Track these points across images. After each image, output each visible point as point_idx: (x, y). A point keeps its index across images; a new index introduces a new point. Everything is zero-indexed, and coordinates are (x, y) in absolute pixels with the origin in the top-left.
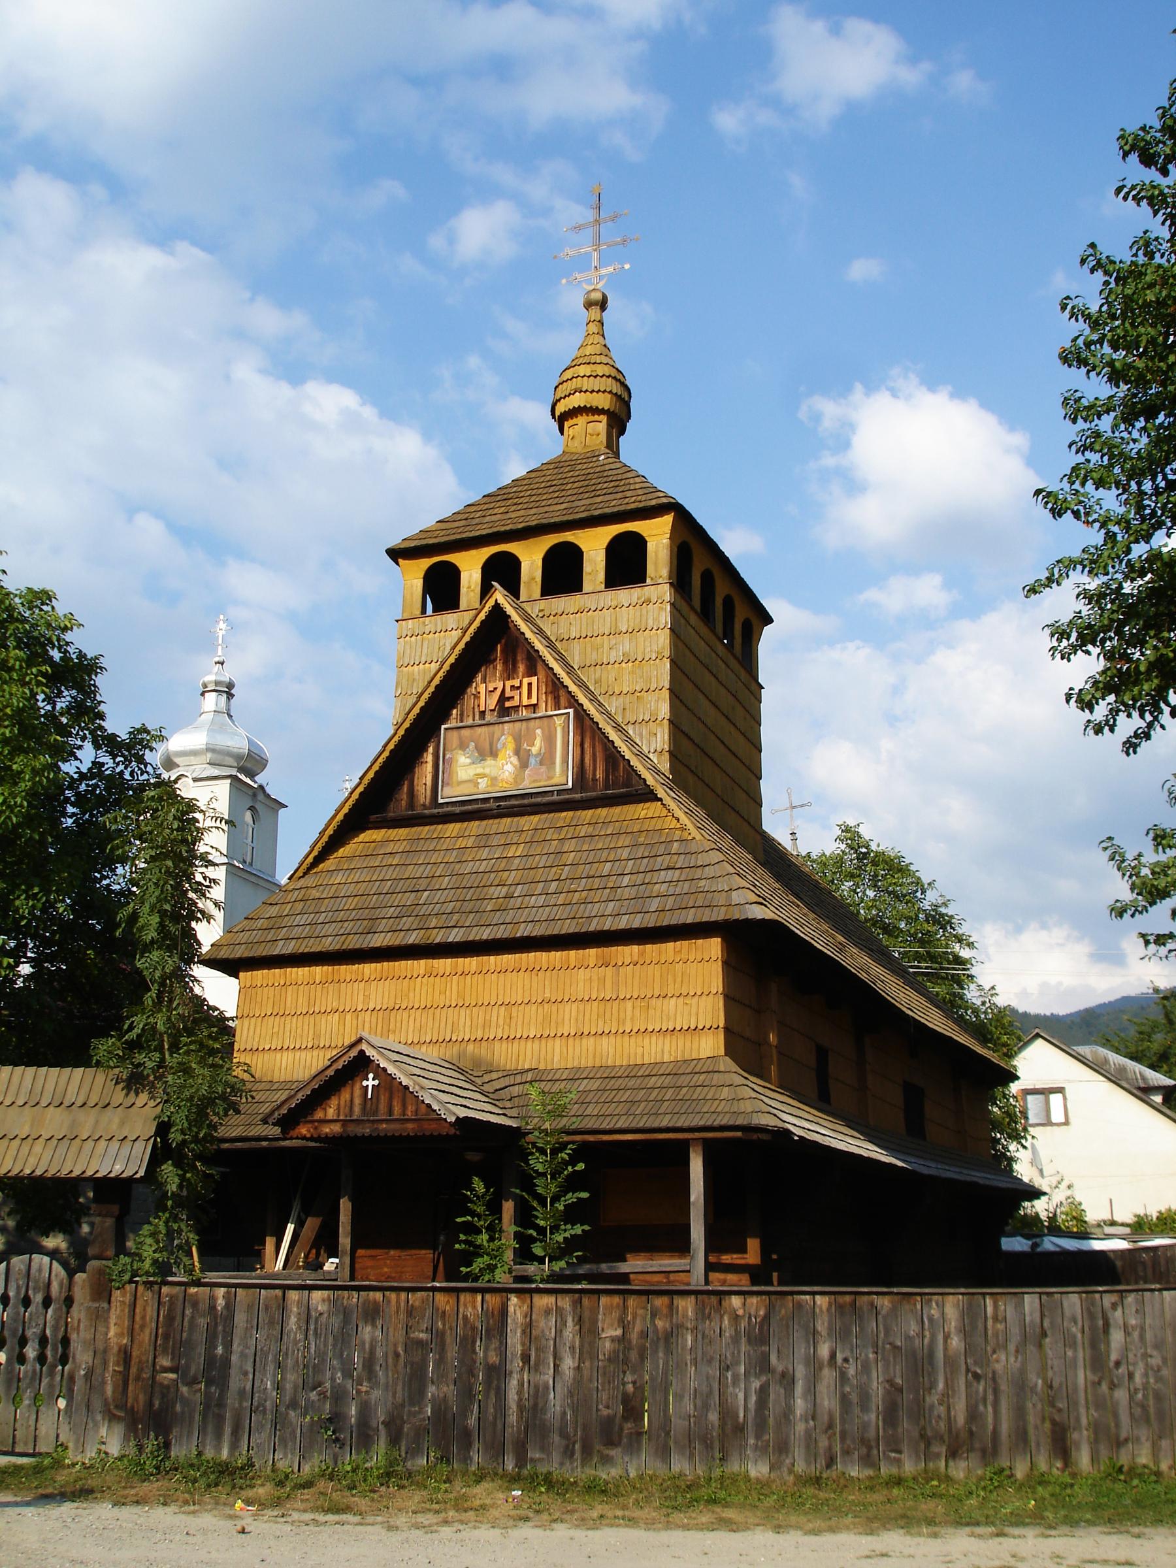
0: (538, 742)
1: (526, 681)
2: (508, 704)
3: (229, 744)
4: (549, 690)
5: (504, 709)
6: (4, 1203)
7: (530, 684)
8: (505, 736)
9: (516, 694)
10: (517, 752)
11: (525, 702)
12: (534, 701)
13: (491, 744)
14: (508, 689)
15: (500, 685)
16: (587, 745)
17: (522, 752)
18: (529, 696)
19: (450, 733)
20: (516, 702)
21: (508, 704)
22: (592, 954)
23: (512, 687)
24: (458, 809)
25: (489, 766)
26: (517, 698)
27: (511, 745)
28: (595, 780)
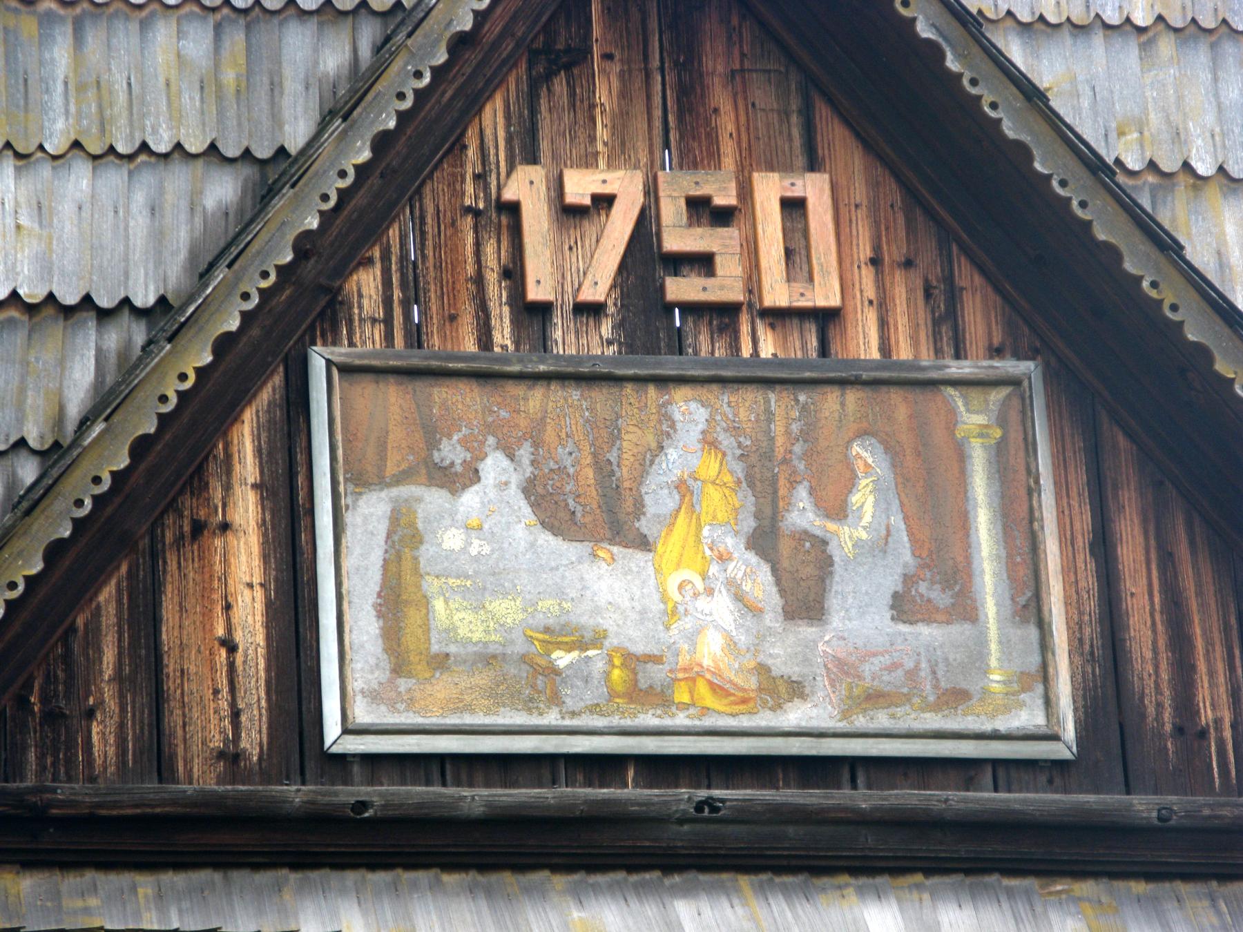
0: (863, 499)
1: (769, 190)
2: (681, 288)
3: (397, 721)
4: (894, 252)
5: (661, 323)
6: (1165, 924)
7: (793, 207)
8: (690, 442)
9: (721, 242)
10: (764, 540)
11: (777, 294)
12: (826, 295)
13: (604, 471)
14: (671, 211)
15: (626, 186)
16: (1132, 550)
17: (785, 547)
18: (796, 255)
19: (366, 393)
20: (725, 285)
21: (681, 288)
22: (980, 388)
23: (702, 210)
24: (476, 797)
25: (611, 591)
26: (730, 270)
27: (723, 508)
28: (1189, 730)
